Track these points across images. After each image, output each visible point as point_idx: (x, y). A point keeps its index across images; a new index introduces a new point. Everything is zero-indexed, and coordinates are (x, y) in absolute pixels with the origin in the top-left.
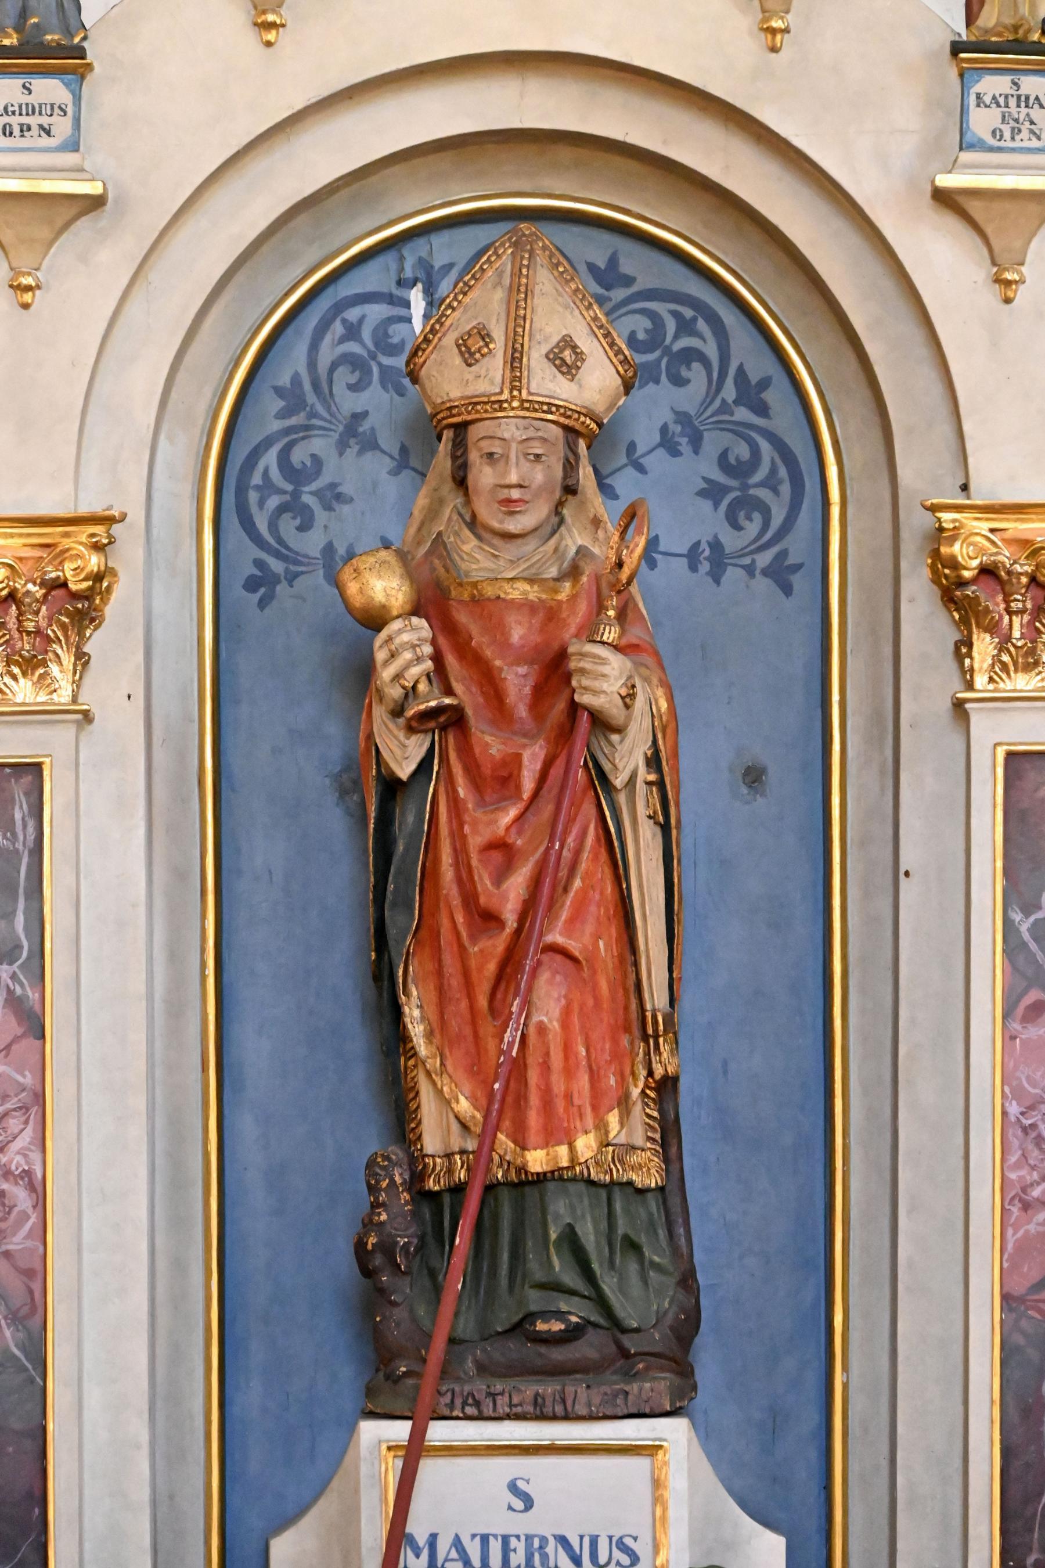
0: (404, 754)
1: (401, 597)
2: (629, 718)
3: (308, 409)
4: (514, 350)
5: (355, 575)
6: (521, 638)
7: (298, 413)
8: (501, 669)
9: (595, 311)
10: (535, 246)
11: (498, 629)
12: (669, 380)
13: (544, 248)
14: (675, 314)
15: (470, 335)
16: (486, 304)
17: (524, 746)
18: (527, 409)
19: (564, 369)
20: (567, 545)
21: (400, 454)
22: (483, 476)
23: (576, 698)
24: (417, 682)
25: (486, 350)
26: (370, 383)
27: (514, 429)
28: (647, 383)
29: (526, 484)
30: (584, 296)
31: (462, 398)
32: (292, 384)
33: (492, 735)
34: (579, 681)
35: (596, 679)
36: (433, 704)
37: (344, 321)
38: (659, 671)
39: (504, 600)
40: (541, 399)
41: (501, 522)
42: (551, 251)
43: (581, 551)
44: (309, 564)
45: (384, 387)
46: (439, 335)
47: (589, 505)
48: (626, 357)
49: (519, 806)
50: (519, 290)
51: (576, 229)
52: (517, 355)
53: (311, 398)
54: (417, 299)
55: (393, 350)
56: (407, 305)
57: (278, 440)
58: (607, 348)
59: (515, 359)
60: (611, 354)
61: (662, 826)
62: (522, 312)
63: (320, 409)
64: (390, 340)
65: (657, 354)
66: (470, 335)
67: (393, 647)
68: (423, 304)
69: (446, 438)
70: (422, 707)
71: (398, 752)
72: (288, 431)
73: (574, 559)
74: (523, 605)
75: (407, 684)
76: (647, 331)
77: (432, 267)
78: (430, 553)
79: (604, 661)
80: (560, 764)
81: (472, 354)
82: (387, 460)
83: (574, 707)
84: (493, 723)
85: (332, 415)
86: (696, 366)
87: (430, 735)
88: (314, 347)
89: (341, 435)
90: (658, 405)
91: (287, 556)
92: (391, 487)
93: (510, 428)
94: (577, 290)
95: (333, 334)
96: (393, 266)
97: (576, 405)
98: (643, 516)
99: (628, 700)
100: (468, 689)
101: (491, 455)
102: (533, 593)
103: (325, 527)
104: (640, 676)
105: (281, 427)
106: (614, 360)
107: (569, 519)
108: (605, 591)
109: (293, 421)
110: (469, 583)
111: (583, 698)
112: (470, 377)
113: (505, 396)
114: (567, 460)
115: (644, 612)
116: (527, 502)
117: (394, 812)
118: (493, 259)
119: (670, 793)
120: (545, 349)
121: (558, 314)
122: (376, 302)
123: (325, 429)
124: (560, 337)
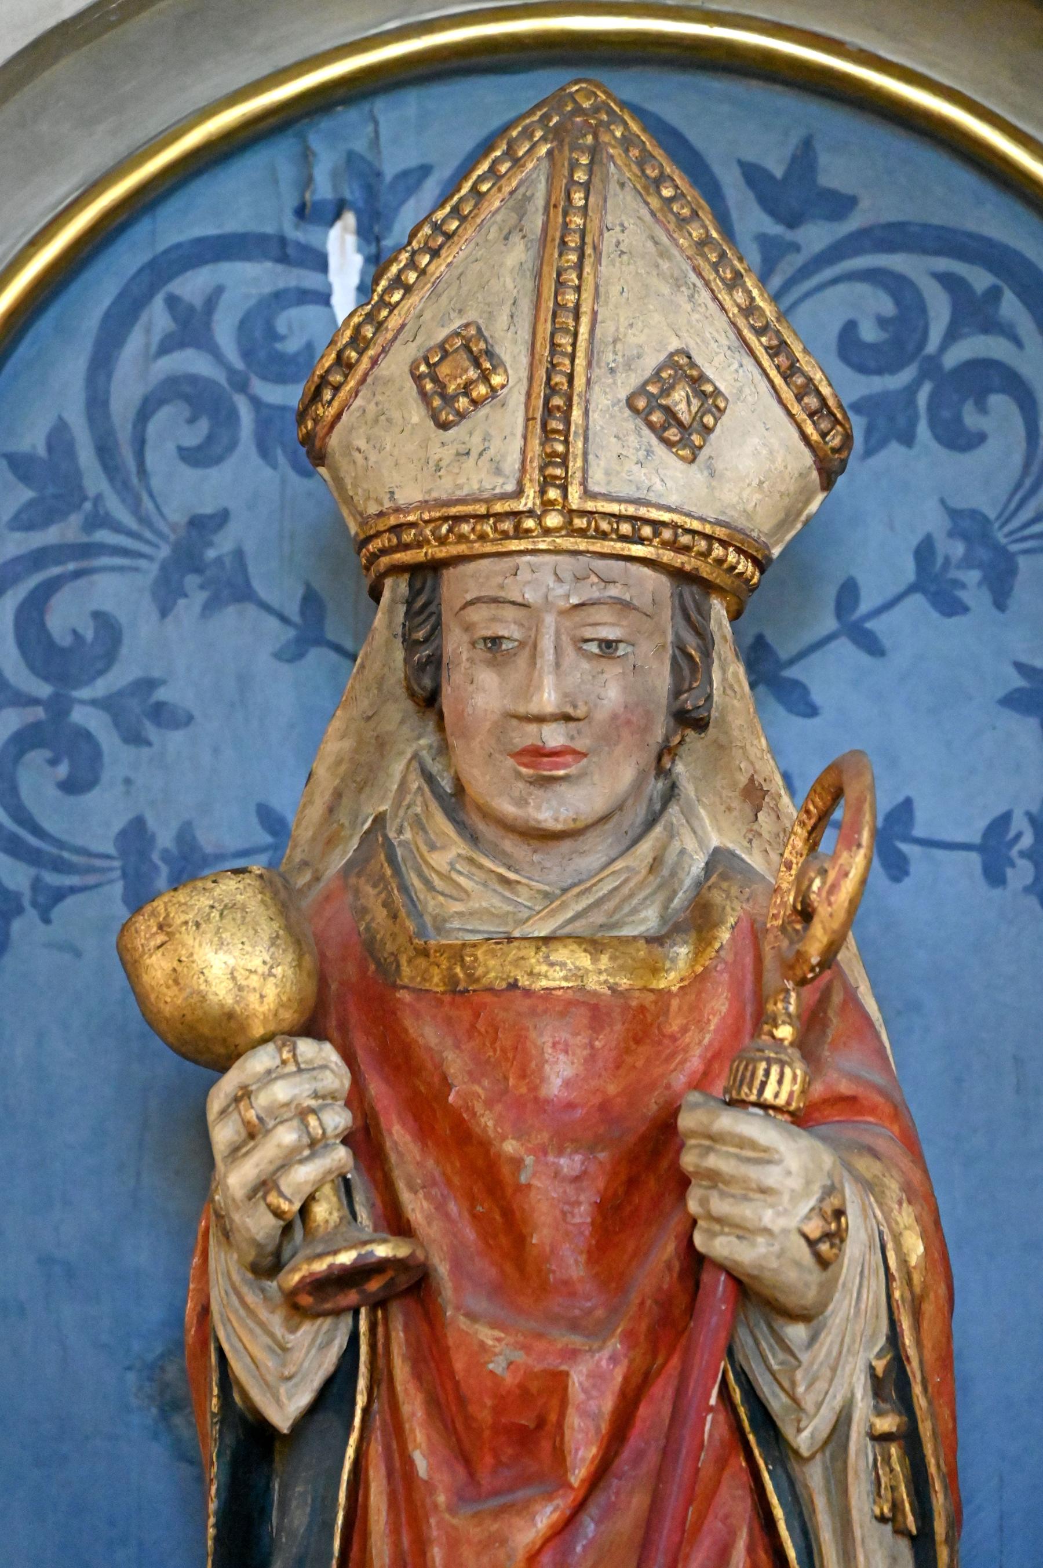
0: (284, 1370)
1: (271, 991)
2: (827, 1290)
3: (88, 506)
4: (552, 390)
5: (160, 938)
6: (567, 1084)
7: (64, 515)
8: (517, 1163)
9: (749, 293)
10: (605, 138)
11: (510, 1059)
12: (938, 438)
13: (627, 142)
14: (948, 281)
15: (446, 354)
16: (486, 277)
17: (572, 1354)
18: (582, 533)
19: (673, 434)
20: (683, 852)
21: (303, 613)
22: (480, 692)
23: (698, 1240)
24: (311, 1199)
25: (482, 390)
26: (232, 445)
27: (551, 581)
28: (883, 443)
29: (580, 713)
30: (723, 255)
31: (424, 505)
32: (50, 448)
33: (494, 1325)
34: (704, 1202)
35: (746, 1198)
36: (346, 1258)
37: (172, 302)
38: (905, 1162)
39: (527, 992)
40: (614, 508)
41: (522, 802)
42: (644, 149)
43: (721, 863)
44: (89, 870)
45: (264, 452)
46: (371, 352)
47: (737, 753)
48: (823, 400)
49: (559, 1502)
50: (563, 243)
51: (718, 84)
52: (557, 401)
53: (95, 481)
54: (343, 242)
55: (282, 368)
56: (322, 264)
57: (16, 580)
58: (778, 380)
59: (553, 412)
60: (787, 395)
61: (912, 1538)
62: (571, 297)
63: (116, 508)
64: (279, 346)
65: (906, 376)
66: (446, 354)
67: (251, 1115)
68: (357, 261)
69: (403, 584)
70: (320, 1266)
71: (269, 1363)
72: (38, 558)
73: (699, 885)
74: (570, 1003)
75: (285, 1206)
76: (882, 322)
77: (379, 174)
78: (356, 866)
79: (765, 1157)
80: (662, 1391)
81: (449, 400)
82: (273, 623)
83: (694, 1262)
84: (497, 1290)
85: (144, 520)
86: (998, 401)
87: (348, 1320)
88: (102, 362)
89: (164, 568)
90: (910, 494)
91: (38, 851)
92: (282, 688)
93: (541, 578)
94: (705, 242)
95: (148, 331)
96: (287, 172)
97: (702, 520)
98: (860, 801)
99: (824, 1247)
100: (440, 1207)
101: (495, 641)
102: (597, 973)
103: (128, 781)
104: (859, 1179)
105: (23, 550)
106: (796, 409)
107: (688, 788)
108: (772, 975)
109: (50, 536)
110: (442, 949)
111: (718, 1246)
112: (447, 454)
113: (529, 500)
114: (680, 647)
115: (871, 1006)
116: (585, 755)
117: (268, 1489)
118: (503, 168)
119: (932, 1461)
120: (626, 384)
121: (658, 301)
122: (248, 258)
123: (125, 552)
124: (662, 357)
